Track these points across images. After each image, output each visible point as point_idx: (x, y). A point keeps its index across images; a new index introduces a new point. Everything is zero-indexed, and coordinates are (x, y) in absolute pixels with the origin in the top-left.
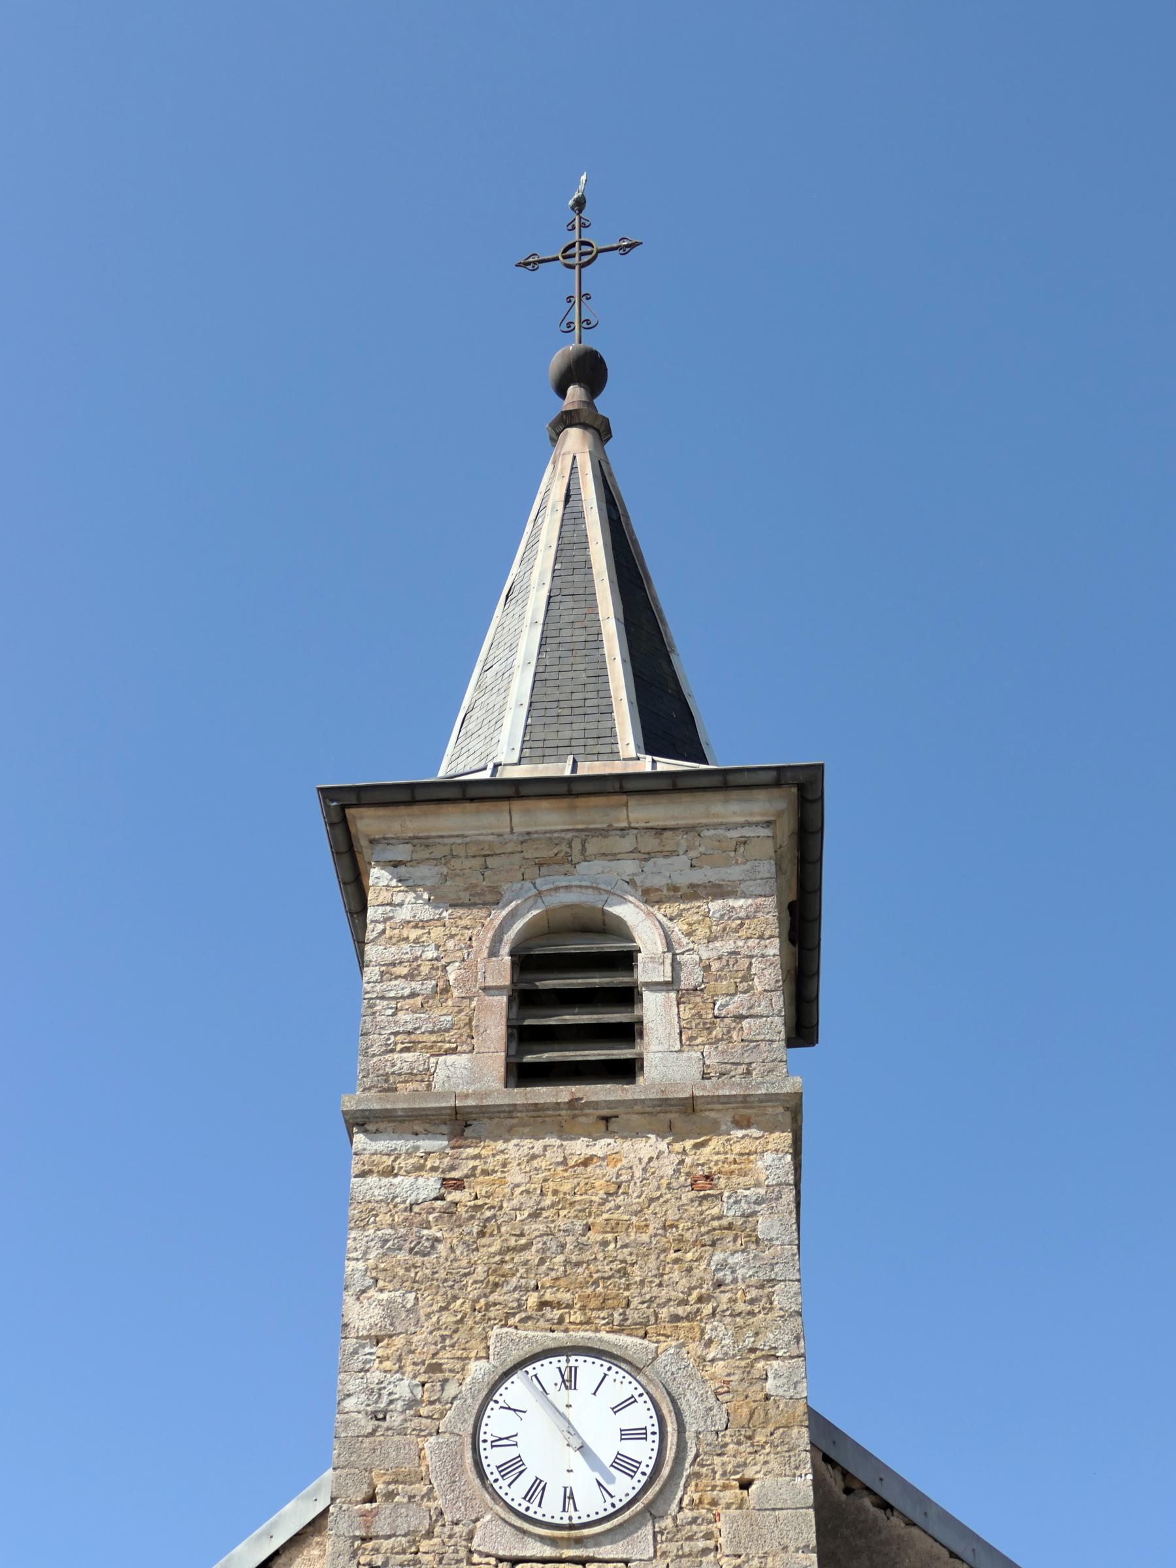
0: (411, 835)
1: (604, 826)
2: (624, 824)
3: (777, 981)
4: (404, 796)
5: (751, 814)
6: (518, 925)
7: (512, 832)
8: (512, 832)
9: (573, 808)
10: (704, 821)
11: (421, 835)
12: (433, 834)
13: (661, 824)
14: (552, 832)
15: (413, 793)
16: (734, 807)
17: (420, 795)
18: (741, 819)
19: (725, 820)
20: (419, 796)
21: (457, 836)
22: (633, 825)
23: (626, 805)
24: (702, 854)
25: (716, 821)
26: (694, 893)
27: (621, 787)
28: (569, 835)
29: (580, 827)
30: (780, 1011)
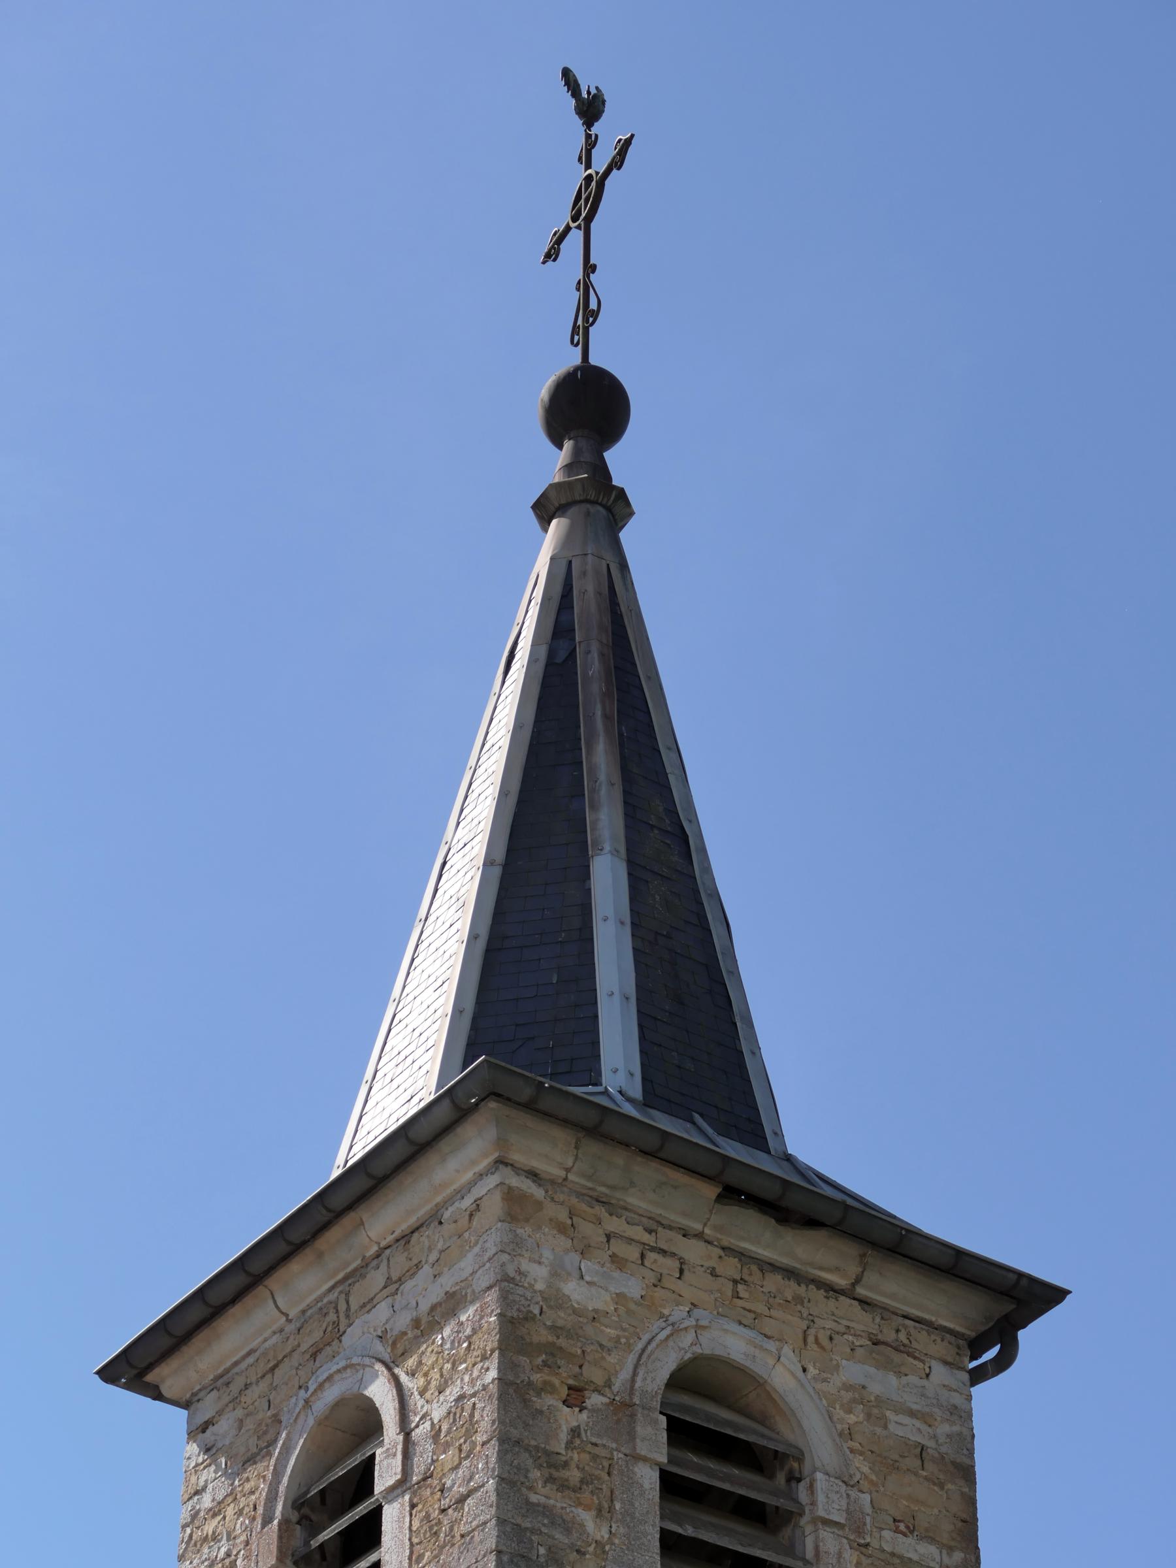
0: (211, 1377)
1: (359, 1262)
2: (375, 1248)
3: (494, 1422)
4: (240, 1280)
5: (474, 1163)
6: (285, 1480)
7: (289, 1321)
8: (289, 1321)
9: (320, 1255)
10: (439, 1199)
11: (220, 1371)
12: (228, 1364)
13: (404, 1227)
14: (318, 1300)
15: (206, 1303)
16: (452, 1164)
17: (256, 1267)
18: (469, 1175)
19: (455, 1186)
20: (179, 1331)
21: (249, 1354)
22: (383, 1244)
23: (362, 1223)
24: (441, 1252)
25: (449, 1191)
26: (425, 1327)
27: (289, 1243)
28: (332, 1296)
29: (340, 1276)
30: (493, 1470)
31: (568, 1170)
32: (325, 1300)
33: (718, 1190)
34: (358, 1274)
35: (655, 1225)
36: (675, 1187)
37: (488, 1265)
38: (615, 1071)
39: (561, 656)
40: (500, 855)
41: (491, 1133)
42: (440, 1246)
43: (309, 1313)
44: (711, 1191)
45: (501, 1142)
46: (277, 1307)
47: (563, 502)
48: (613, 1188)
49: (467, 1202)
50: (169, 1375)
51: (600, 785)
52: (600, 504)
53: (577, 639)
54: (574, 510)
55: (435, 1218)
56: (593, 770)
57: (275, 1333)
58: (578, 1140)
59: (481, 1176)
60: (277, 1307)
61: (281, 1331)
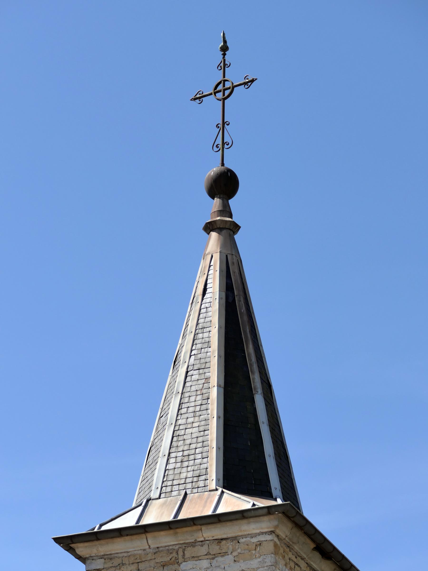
0: (103, 554)
1: (193, 541)
5: (262, 528)
9: (176, 533)
14: (169, 546)
18: (258, 531)
19: (250, 533)
23: (201, 530)
24: (239, 553)
31: (286, 536)
32: (171, 547)
33: (315, 546)
34: (193, 544)
35: (298, 555)
36: (306, 544)
37: (266, 568)
38: (276, 489)
39: (230, 300)
40: (222, 384)
41: (276, 523)
42: (239, 551)
43: (161, 549)
44: (313, 546)
45: (276, 527)
46: (148, 543)
47: (221, 227)
48: (293, 543)
49: (254, 540)
50: (82, 549)
51: (253, 363)
52: (233, 231)
53: (236, 294)
54: (224, 232)
55: (235, 539)
56: (249, 355)
57: (141, 550)
58: (293, 527)
59: (262, 533)
60: (148, 543)
61: (144, 550)
